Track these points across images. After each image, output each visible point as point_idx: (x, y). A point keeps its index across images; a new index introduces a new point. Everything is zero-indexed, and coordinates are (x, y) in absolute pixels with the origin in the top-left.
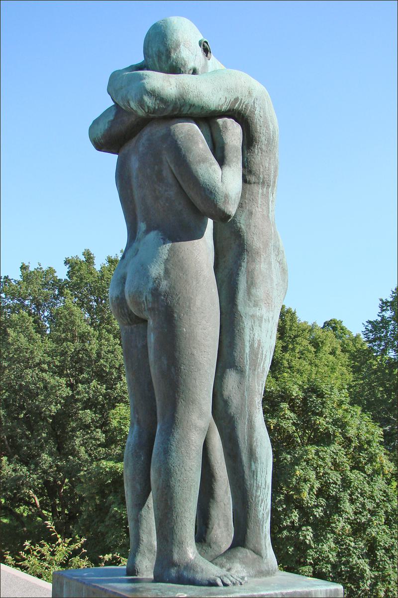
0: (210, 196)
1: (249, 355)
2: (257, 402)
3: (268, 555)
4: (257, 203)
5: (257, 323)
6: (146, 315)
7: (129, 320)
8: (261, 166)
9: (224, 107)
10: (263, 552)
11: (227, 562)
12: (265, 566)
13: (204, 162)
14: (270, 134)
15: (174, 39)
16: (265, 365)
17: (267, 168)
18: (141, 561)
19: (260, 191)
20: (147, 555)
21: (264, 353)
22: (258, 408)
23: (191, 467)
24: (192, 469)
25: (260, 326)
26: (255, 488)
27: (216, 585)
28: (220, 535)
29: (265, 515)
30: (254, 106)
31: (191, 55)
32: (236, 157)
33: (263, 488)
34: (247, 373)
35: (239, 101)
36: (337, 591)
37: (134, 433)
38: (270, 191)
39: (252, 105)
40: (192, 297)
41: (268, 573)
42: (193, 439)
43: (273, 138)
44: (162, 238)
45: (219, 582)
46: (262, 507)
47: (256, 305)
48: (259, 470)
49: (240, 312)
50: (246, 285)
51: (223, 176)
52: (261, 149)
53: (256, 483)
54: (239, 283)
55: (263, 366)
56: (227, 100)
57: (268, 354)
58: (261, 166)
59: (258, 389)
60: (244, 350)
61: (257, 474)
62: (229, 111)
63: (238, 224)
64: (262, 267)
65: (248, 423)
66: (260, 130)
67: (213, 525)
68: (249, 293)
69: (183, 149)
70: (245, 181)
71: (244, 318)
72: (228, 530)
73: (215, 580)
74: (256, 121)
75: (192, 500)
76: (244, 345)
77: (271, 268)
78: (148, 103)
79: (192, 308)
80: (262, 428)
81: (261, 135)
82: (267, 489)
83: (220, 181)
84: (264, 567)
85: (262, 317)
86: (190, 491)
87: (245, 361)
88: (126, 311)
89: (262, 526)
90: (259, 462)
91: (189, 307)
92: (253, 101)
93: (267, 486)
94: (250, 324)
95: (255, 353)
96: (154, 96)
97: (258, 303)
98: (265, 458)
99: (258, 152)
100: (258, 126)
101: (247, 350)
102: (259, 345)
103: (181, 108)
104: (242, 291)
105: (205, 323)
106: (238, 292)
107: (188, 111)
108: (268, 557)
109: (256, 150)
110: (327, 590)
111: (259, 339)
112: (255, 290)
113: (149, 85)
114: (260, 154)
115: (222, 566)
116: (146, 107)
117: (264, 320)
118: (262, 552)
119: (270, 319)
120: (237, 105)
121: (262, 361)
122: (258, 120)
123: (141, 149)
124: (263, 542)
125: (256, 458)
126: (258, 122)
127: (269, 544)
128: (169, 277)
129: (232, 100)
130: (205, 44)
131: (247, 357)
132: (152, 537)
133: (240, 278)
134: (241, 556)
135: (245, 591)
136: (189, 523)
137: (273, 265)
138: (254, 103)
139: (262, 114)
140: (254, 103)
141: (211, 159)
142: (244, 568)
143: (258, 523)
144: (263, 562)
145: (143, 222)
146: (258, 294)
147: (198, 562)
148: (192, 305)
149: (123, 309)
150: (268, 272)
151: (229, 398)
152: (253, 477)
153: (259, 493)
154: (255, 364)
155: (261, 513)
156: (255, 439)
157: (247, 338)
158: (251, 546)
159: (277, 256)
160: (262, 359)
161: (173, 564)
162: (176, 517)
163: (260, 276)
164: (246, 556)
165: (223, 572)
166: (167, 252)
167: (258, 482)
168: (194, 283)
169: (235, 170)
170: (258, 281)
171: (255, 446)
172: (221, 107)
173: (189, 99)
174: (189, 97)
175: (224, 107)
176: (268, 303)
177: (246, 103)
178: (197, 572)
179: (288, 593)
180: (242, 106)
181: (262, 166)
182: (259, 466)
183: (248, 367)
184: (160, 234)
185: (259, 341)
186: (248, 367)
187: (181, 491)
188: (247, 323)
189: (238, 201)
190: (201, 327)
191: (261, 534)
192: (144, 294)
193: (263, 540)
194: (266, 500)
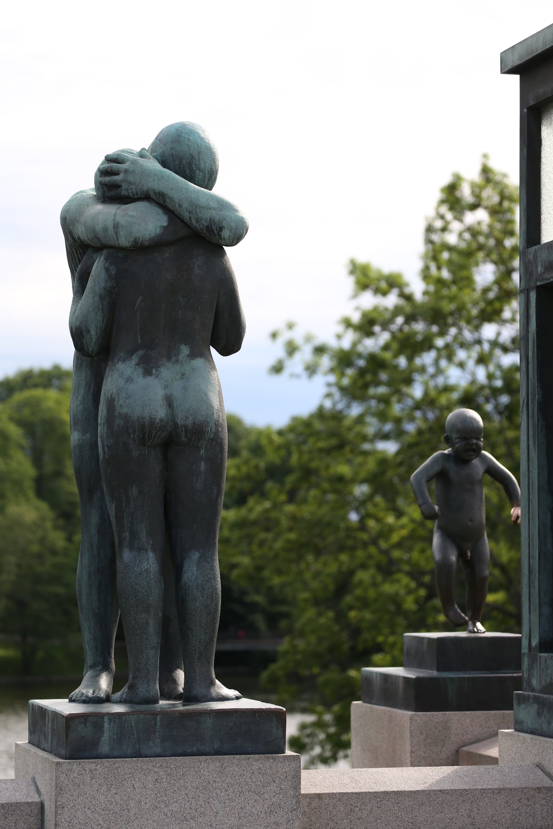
192: (211, 425)
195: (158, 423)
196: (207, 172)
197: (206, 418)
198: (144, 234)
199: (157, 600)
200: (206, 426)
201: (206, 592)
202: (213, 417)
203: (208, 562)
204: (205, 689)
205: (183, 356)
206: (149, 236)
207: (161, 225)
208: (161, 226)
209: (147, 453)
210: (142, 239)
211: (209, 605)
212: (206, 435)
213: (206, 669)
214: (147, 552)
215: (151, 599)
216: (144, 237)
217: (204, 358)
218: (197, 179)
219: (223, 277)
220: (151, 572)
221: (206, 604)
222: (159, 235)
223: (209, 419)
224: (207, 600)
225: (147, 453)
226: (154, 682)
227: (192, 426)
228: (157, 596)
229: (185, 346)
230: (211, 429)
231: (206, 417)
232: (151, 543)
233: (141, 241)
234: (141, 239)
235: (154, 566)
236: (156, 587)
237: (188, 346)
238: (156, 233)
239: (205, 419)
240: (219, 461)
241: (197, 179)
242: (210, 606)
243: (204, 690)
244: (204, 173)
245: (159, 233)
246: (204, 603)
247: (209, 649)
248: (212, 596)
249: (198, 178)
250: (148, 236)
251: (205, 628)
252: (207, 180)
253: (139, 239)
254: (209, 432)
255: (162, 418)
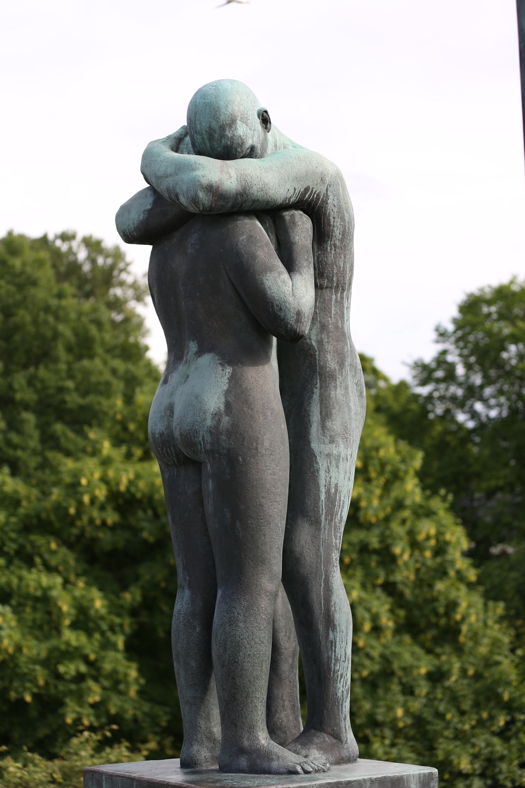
0: (279, 313)
1: (325, 502)
2: (334, 559)
3: (349, 739)
4: (330, 312)
5: (334, 463)
6: (202, 457)
7: (176, 461)
8: (335, 266)
9: (292, 200)
10: (343, 735)
11: (302, 748)
12: (345, 751)
13: (271, 271)
14: (345, 226)
15: (228, 113)
16: (343, 514)
17: (342, 269)
18: (199, 751)
19: (334, 297)
20: (206, 744)
21: (342, 499)
22: (336, 566)
23: (262, 639)
24: (263, 642)
25: (337, 467)
26: (333, 661)
27: (296, 773)
28: (285, 719)
29: (345, 693)
30: (327, 194)
31: (249, 130)
32: (307, 260)
33: (343, 661)
34: (323, 524)
35: (310, 190)
36: (431, 774)
37: (185, 600)
38: (345, 296)
39: (324, 194)
40: (259, 436)
41: (349, 760)
42: (263, 606)
43: (349, 229)
44: (220, 364)
45: (299, 769)
46: (342, 684)
47: (332, 441)
48: (338, 639)
49: (313, 450)
50: (319, 416)
51: (294, 288)
52: (335, 246)
53: (335, 656)
54: (311, 414)
55: (341, 515)
56: (296, 192)
57: (346, 499)
58: (335, 266)
59: (336, 543)
60: (319, 498)
61: (335, 644)
62: (298, 202)
63: (308, 340)
64: (338, 393)
65: (325, 584)
66: (334, 223)
67: (278, 707)
68: (323, 427)
69: (245, 255)
70: (318, 287)
71: (318, 457)
72: (294, 713)
73: (295, 767)
74: (329, 213)
75: (264, 677)
76: (319, 490)
77: (348, 394)
78: (204, 200)
79: (259, 450)
80: (340, 590)
81: (335, 229)
82: (347, 662)
83: (291, 294)
84: (345, 753)
85: (339, 456)
86: (262, 667)
87: (321, 510)
88: (173, 450)
89: (342, 705)
90: (338, 630)
91: (256, 449)
92: (325, 188)
93: (347, 658)
94: (325, 465)
95: (332, 500)
96: (211, 192)
97: (334, 438)
98: (345, 624)
99: (331, 249)
100: (331, 218)
101: (323, 496)
102: (336, 490)
103: (242, 204)
104: (315, 424)
105: (275, 466)
106: (311, 426)
107: (250, 207)
108: (349, 741)
109: (329, 248)
110: (420, 774)
111: (336, 482)
112: (330, 423)
113: (205, 179)
114: (333, 252)
115: (296, 752)
116: (201, 204)
117: (341, 459)
118: (342, 735)
119: (349, 457)
120: (307, 196)
121: (340, 508)
122: (331, 211)
123: (190, 251)
124: (342, 724)
125: (335, 625)
126: (332, 213)
127: (349, 727)
128: (231, 412)
129: (302, 190)
130: (265, 114)
131: (322, 505)
132: (211, 723)
133: (312, 409)
134: (317, 741)
135: (330, 778)
136: (260, 704)
137: (350, 389)
138: (327, 190)
139: (336, 203)
140: (327, 190)
141: (279, 266)
142: (322, 754)
143: (337, 703)
144: (343, 748)
145: (193, 341)
146: (335, 427)
147: (272, 749)
148: (259, 446)
149: (170, 449)
150: (344, 399)
151: (301, 554)
152: (332, 648)
153: (338, 668)
154: (331, 513)
155: (340, 691)
156: (333, 603)
157: (322, 482)
158: (329, 730)
159: (354, 376)
160: (340, 507)
161: (242, 751)
162: (246, 697)
163: (335, 405)
164: (324, 741)
165: (301, 759)
166: (227, 381)
167: (336, 654)
168: (261, 418)
169: (306, 278)
170: (334, 411)
171: (333, 611)
172: (289, 200)
173: (253, 194)
174: (253, 192)
175: (292, 200)
176: (346, 438)
177: (318, 191)
178: (272, 759)
179: (378, 778)
180: (313, 196)
181: (336, 266)
182: (338, 635)
183: (323, 517)
184: (217, 358)
185: (336, 485)
186: (323, 517)
187: (251, 668)
188: (322, 464)
189: (311, 317)
190: (270, 472)
191: (341, 715)
192: (201, 433)
193: (343, 722)
194: (346, 675)
195: (158, 438)
196: (204, 132)
197: (193, 426)
198: (129, 225)
199: (186, 646)
200: (194, 435)
201: (219, 639)
202: (204, 423)
203: (227, 602)
204: (229, 757)
205: (191, 355)
206: (133, 226)
207: (144, 210)
208: (145, 211)
209: (176, 474)
210: (129, 230)
211: (222, 655)
212: (199, 447)
213: (232, 733)
214: (184, 590)
215: (179, 645)
216: (129, 227)
217: (214, 352)
218: (197, 143)
219: (222, 250)
220: (181, 613)
221: (218, 654)
222: (144, 221)
223: (197, 427)
224: (219, 648)
225: (176, 474)
226: (190, 743)
227: (180, 438)
228: (185, 642)
229: (193, 342)
230: (203, 439)
231: (193, 424)
232: (188, 579)
233: (129, 233)
234: (127, 230)
235: (186, 607)
236: (184, 631)
237: (196, 341)
238: (140, 220)
239: (192, 427)
240: (229, 477)
241: (197, 143)
242: (222, 657)
243: (228, 758)
244: (202, 134)
245: (143, 219)
246: (217, 653)
247: (231, 709)
248: (226, 645)
249: (198, 142)
250: (132, 227)
251: (221, 683)
252: (207, 141)
253: (127, 232)
254: (201, 443)
255: (161, 432)
